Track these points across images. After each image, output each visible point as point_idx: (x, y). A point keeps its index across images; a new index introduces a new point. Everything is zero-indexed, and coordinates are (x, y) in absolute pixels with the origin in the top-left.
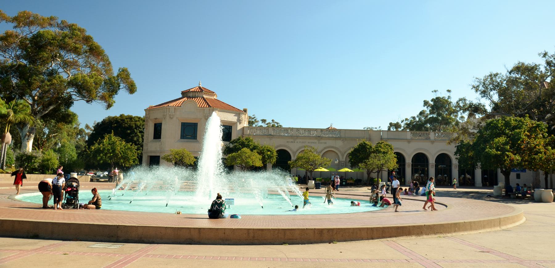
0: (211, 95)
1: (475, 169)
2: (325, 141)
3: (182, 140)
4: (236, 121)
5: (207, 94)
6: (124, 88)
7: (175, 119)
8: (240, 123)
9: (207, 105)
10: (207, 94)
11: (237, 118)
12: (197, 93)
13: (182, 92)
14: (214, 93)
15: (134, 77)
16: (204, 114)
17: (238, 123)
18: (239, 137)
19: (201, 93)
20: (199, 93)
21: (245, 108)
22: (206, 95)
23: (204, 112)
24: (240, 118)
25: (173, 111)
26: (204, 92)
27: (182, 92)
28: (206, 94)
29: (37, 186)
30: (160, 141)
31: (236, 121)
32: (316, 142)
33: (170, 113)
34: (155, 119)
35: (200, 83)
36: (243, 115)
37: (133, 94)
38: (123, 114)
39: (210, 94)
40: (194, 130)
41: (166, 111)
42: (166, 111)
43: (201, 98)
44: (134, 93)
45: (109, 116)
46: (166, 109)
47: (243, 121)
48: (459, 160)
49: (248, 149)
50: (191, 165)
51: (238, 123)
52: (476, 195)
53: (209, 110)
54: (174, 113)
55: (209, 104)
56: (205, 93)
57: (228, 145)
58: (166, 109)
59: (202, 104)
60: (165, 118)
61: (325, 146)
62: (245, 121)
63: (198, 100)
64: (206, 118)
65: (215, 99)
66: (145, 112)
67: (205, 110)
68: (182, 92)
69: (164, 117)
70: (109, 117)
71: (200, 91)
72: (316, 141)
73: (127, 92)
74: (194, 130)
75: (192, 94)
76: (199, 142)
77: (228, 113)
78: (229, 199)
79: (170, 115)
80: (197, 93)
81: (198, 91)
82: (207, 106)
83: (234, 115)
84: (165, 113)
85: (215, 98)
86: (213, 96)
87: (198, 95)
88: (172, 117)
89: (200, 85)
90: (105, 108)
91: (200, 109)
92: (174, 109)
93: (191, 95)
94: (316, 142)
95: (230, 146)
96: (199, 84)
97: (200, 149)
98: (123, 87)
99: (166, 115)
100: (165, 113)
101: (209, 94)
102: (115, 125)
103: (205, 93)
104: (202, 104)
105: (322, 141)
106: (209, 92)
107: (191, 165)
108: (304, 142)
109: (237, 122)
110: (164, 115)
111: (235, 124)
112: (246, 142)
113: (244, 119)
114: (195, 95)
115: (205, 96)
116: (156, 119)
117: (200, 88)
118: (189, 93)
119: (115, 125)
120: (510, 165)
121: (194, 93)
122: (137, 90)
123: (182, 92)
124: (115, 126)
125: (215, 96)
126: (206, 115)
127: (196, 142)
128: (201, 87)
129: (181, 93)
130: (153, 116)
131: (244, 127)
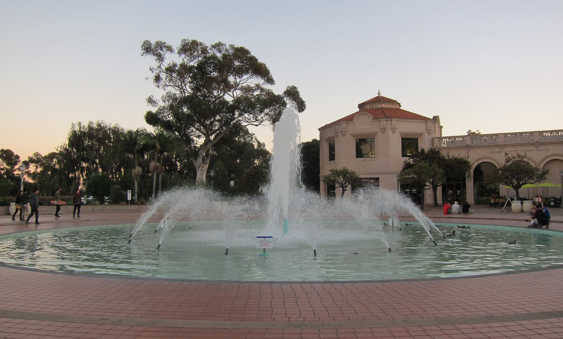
1: (467, 203)
2: (546, 147)
7: (347, 135)
15: (303, 96)
29: (71, 214)
32: (533, 150)
33: (342, 130)
43: (381, 110)
48: (69, 138)
50: (378, 185)
57: (408, 161)
61: (548, 153)
66: (319, 132)
69: (336, 134)
72: (533, 148)
78: (264, 237)
79: (342, 132)
90: (100, 122)
94: (533, 150)
95: (410, 161)
97: (47, 168)
98: (290, 106)
101: (389, 103)
105: (542, 148)
107: (378, 185)
108: (513, 151)
110: (336, 133)
120: (4, 163)
130: (326, 136)
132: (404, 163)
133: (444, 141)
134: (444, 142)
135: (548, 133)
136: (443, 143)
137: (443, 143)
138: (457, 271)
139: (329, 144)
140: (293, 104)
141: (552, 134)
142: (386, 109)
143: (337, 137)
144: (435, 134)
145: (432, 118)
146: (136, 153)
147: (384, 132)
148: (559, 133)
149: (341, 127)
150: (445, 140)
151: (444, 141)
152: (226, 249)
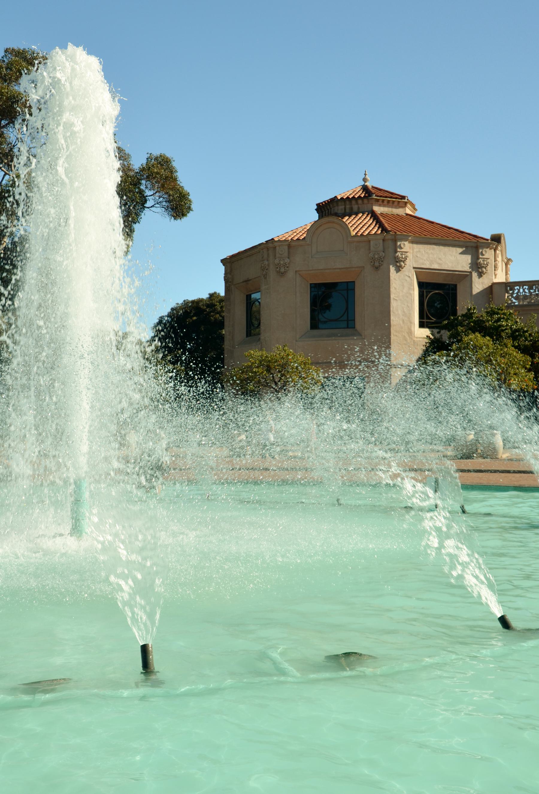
0: (396, 203)
3: (315, 332)
4: (467, 268)
5: (383, 201)
6: (157, 205)
7: (291, 274)
8: (480, 275)
9: (379, 228)
10: (383, 201)
11: (470, 261)
12: (357, 203)
13: (317, 205)
14: (403, 197)
16: (371, 255)
17: (475, 275)
18: (469, 310)
19: (365, 201)
20: (360, 201)
21: (496, 232)
22: (380, 205)
23: (370, 249)
24: (478, 258)
25: (286, 254)
26: (374, 196)
27: (317, 205)
28: (382, 203)
30: (259, 339)
31: (467, 268)
34: (246, 281)
35: (367, 173)
36: (488, 250)
37: (184, 219)
38: (215, 293)
39: (394, 201)
40: (347, 302)
41: (268, 255)
42: (268, 255)
44: (184, 215)
45: (184, 301)
46: (268, 249)
47: (490, 268)
49: (484, 336)
51: (475, 275)
52: (470, 495)
53: (383, 240)
54: (287, 260)
55: (386, 225)
56: (377, 200)
58: (268, 249)
59: (366, 229)
60: (265, 276)
62: (496, 267)
63: (356, 219)
64: (377, 264)
65: (407, 214)
67: (372, 243)
68: (318, 205)
70: (186, 303)
71: (365, 196)
73: (167, 216)
74: (347, 302)
75: (343, 207)
76: (361, 335)
77: (442, 247)
80: (357, 203)
81: (359, 197)
82: (380, 232)
83: (460, 250)
84: (266, 262)
85: (408, 211)
86: (402, 207)
87: (359, 208)
88: (282, 270)
89: (365, 182)
91: (358, 242)
92: (287, 247)
93: (340, 209)
96: (365, 180)
99: (268, 265)
100: (266, 262)
102: (195, 318)
103: (377, 200)
104: (364, 229)
106: (391, 197)
109: (471, 272)
111: (465, 277)
112: (488, 321)
113: (491, 261)
114: (351, 209)
115: (378, 209)
116: (247, 281)
117: (365, 188)
118: (335, 204)
119: (195, 318)
121: (348, 202)
122: (192, 206)
123: (318, 205)
124: (193, 321)
125: (408, 205)
126: (376, 256)
127: (354, 335)
128: (370, 187)
129: (316, 207)
131: (494, 284)
132: (427, 341)
133: (516, 291)
134: (517, 293)
135: (525, 287)
136: (515, 295)
137: (515, 295)
138: (492, 564)
139: (247, 296)
140: (161, 199)
141: (532, 289)
142: (382, 214)
143: (265, 278)
144: (495, 275)
145: (489, 237)
146: (29, 169)
147: (377, 268)
148: (516, 288)
149: (275, 256)
150: (519, 290)
151: (516, 291)
152: (139, 650)
